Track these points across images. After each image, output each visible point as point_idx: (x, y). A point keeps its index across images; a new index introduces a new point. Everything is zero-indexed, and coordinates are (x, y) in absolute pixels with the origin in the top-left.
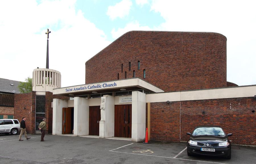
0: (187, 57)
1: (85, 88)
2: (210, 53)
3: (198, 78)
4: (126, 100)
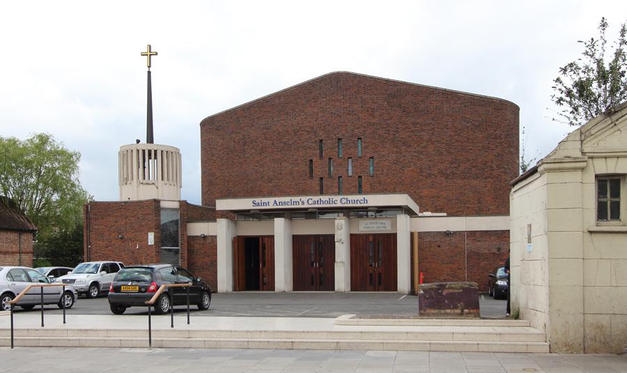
0: (454, 141)
1: (300, 203)
2: (493, 136)
3: (475, 182)
4: (373, 225)
